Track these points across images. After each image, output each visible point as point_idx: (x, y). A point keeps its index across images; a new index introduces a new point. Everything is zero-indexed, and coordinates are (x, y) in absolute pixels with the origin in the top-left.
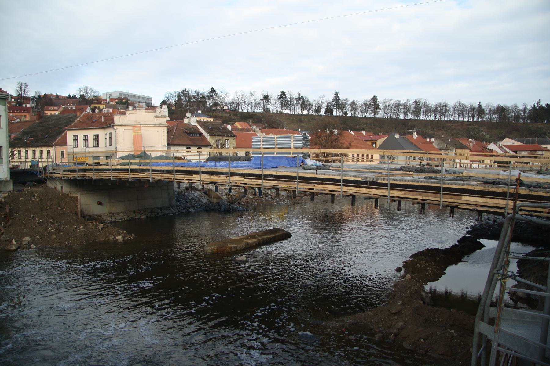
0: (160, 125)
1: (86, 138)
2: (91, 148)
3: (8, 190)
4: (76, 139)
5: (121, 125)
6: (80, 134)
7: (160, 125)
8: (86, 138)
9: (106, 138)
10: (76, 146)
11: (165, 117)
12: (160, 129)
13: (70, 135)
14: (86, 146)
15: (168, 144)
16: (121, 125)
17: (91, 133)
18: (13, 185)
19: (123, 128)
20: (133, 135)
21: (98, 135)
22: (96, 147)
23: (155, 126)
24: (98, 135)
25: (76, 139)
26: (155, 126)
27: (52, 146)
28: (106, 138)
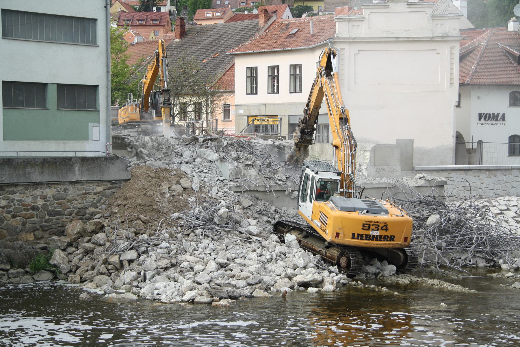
0: (444, 39)
1: (274, 73)
2: (285, 95)
3: (107, 178)
4: (252, 75)
5: (352, 41)
6: (262, 64)
7: (444, 39)
8: (274, 73)
10: (253, 90)
11: (458, 17)
12: (445, 49)
13: (241, 67)
14: (253, 90)
15: (461, 85)
16: (352, 41)
17: (284, 62)
18: (112, 149)
20: (44, 86)
21: (300, 66)
22: (273, 93)
23: (432, 40)
24: (300, 66)
25: (252, 75)
26: (432, 40)
27: (205, 94)
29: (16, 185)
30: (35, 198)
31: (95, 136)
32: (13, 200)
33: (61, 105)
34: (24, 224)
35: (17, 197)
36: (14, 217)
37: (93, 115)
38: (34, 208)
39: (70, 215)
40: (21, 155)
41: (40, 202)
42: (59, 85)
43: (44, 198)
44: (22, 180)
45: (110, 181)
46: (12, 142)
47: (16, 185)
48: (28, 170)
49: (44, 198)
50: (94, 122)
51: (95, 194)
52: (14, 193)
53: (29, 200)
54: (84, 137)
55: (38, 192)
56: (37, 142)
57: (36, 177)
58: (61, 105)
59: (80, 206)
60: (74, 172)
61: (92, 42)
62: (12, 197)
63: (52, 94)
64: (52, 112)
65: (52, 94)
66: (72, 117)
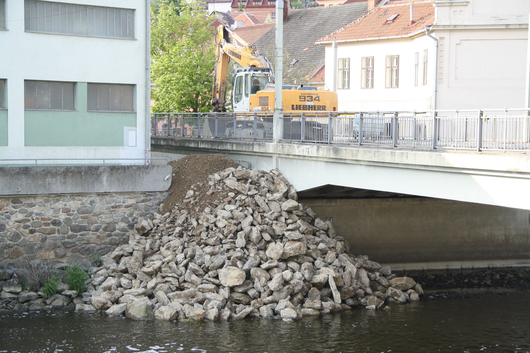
5: (453, 29)
9: (417, 65)
17: (380, 52)
19: (457, 37)
28: (417, 65)
29: (34, 196)
30: (56, 211)
31: (132, 142)
32: (31, 213)
33: (93, 106)
34: (44, 240)
35: (36, 210)
36: (32, 232)
37: (129, 117)
38: (55, 223)
39: (97, 230)
40: (39, 162)
41: (62, 217)
42: (88, 83)
43: (67, 211)
44: (41, 191)
45: (144, 193)
46: (34, 148)
47: (34, 196)
48: (49, 180)
49: (67, 211)
50: (130, 125)
51: (127, 207)
52: (32, 205)
53: (49, 214)
54: (118, 141)
55: (60, 205)
56: (64, 148)
57: (57, 187)
58: (92, 107)
59: (108, 221)
60: (101, 182)
61: (127, 33)
62: (30, 210)
63: (82, 94)
64: (81, 116)
65: (82, 94)
66: (103, 121)
